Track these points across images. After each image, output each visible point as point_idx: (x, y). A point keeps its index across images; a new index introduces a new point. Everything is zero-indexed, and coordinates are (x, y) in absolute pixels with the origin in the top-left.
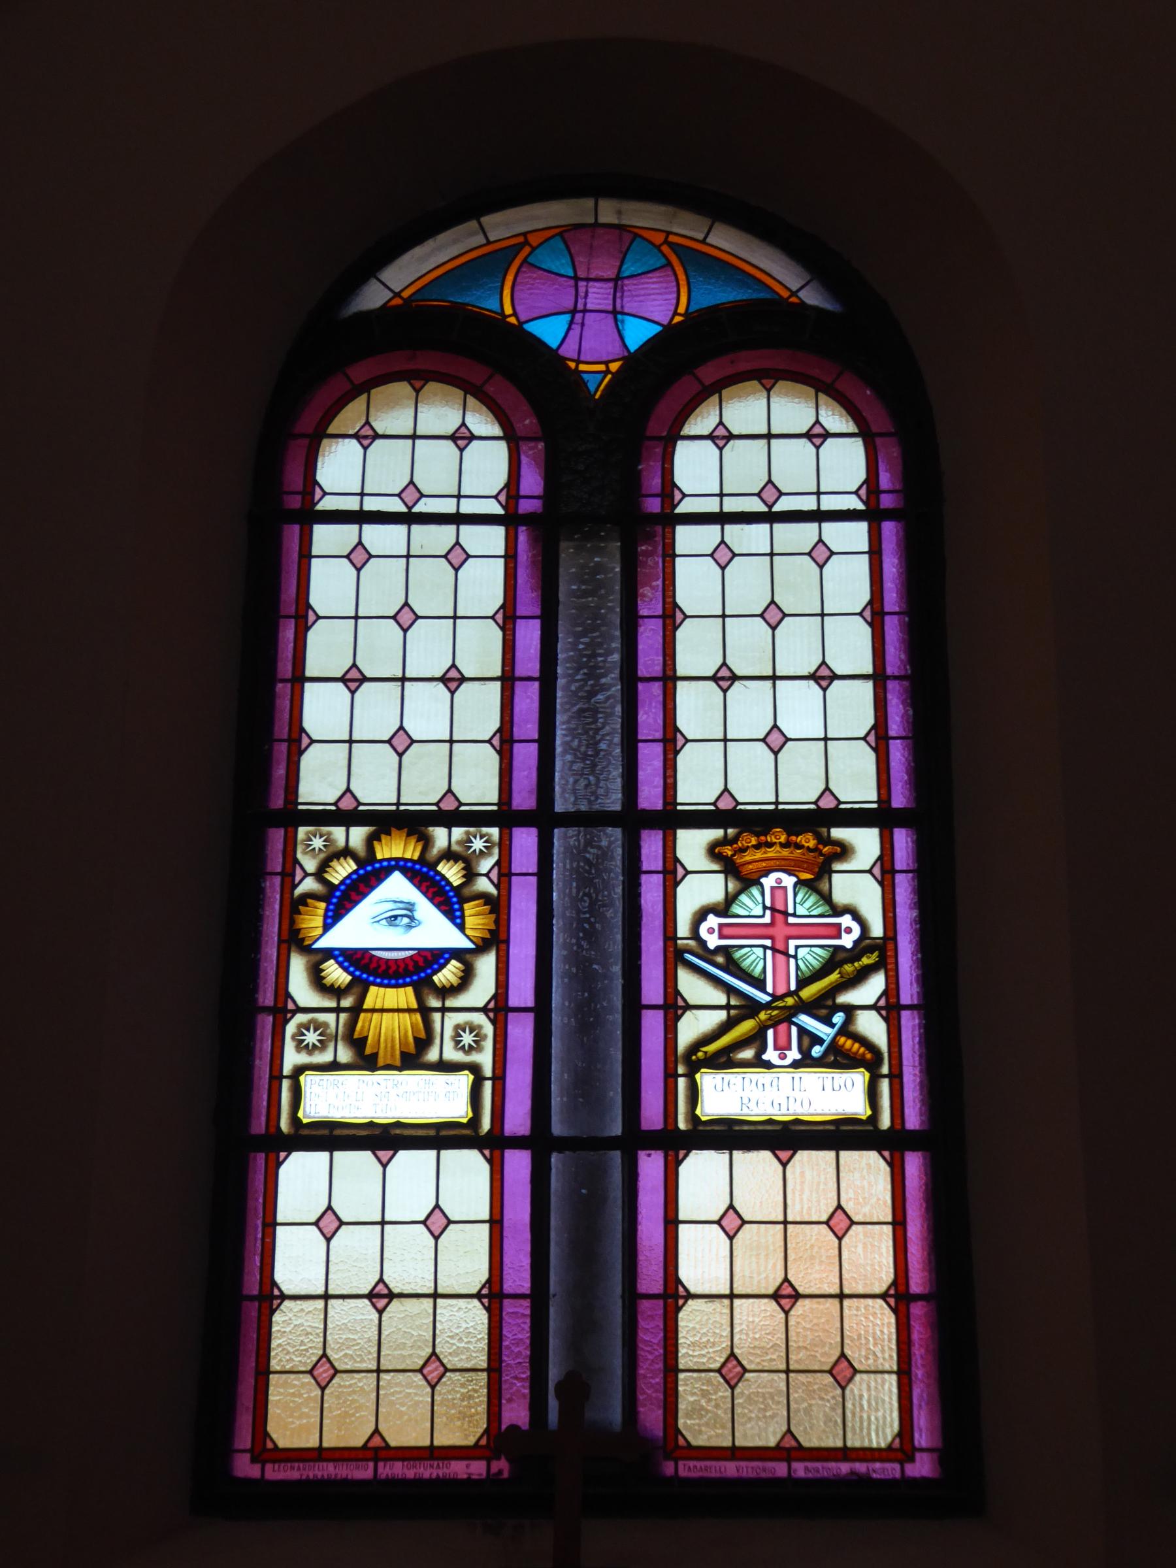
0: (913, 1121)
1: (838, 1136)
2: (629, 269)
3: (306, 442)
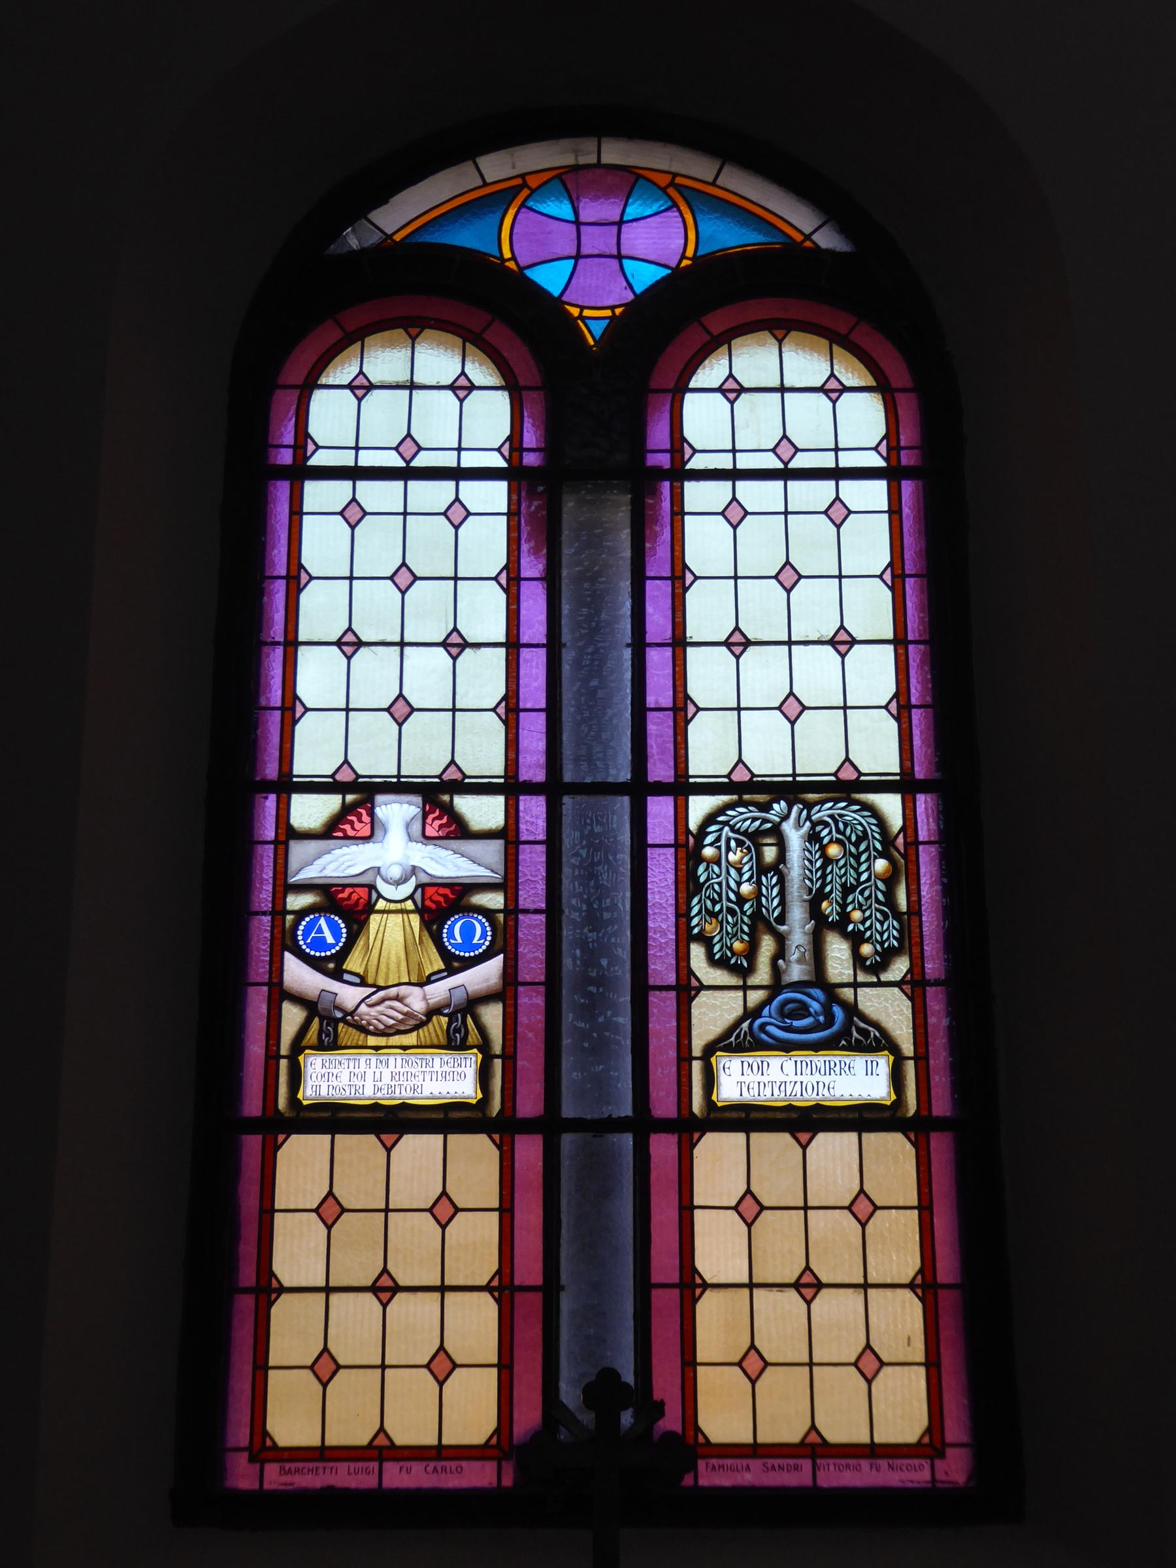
0: (941, 1107)
1: (444, 1119)
2: (632, 211)
3: (296, 393)
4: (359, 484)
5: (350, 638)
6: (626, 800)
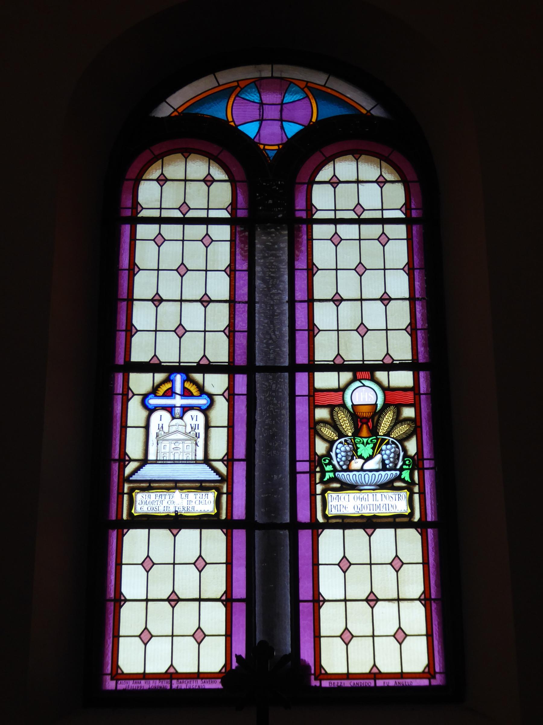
1: (395, 522)
4: (163, 226)
5: (157, 297)
6: (287, 374)
